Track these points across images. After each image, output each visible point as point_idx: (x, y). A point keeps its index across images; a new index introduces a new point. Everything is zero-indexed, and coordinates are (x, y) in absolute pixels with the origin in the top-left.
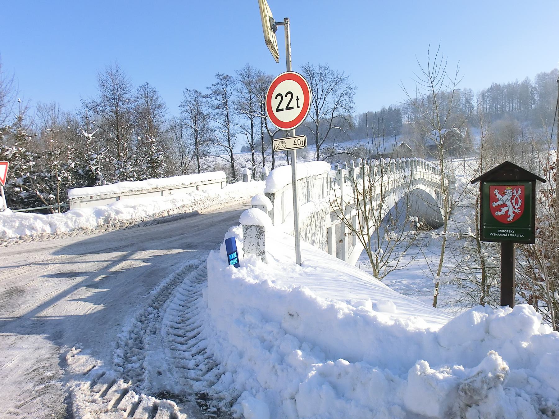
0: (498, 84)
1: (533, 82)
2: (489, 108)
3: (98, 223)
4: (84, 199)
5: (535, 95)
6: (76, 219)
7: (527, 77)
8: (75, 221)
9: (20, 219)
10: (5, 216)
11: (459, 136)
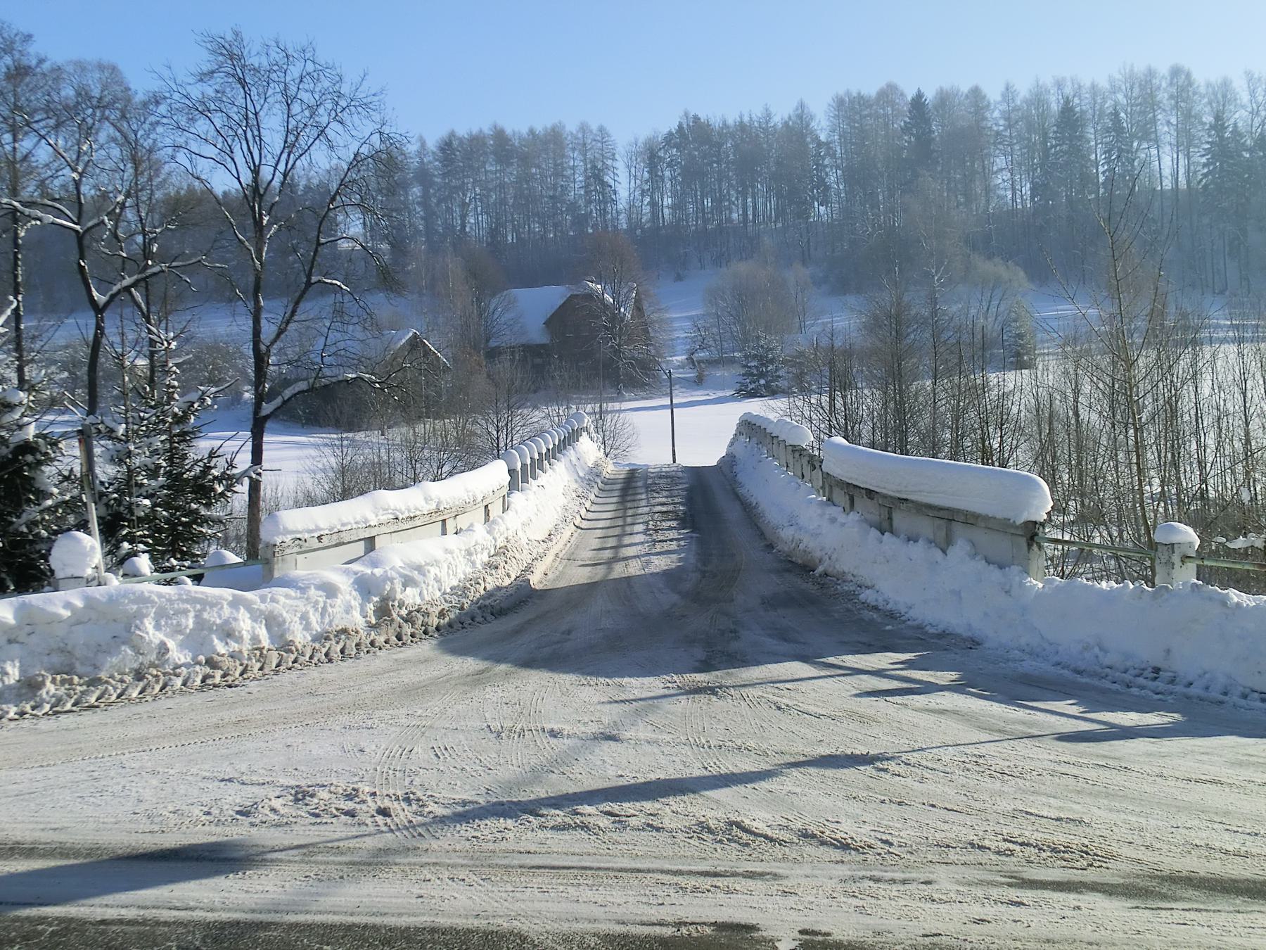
0: (703, 118)
1: (822, 125)
2: (674, 207)
3: (366, 616)
4: (307, 544)
5: (828, 170)
6: (325, 603)
7: (802, 105)
8: (324, 608)
9: (198, 607)
10: (164, 597)
11: (616, 318)
